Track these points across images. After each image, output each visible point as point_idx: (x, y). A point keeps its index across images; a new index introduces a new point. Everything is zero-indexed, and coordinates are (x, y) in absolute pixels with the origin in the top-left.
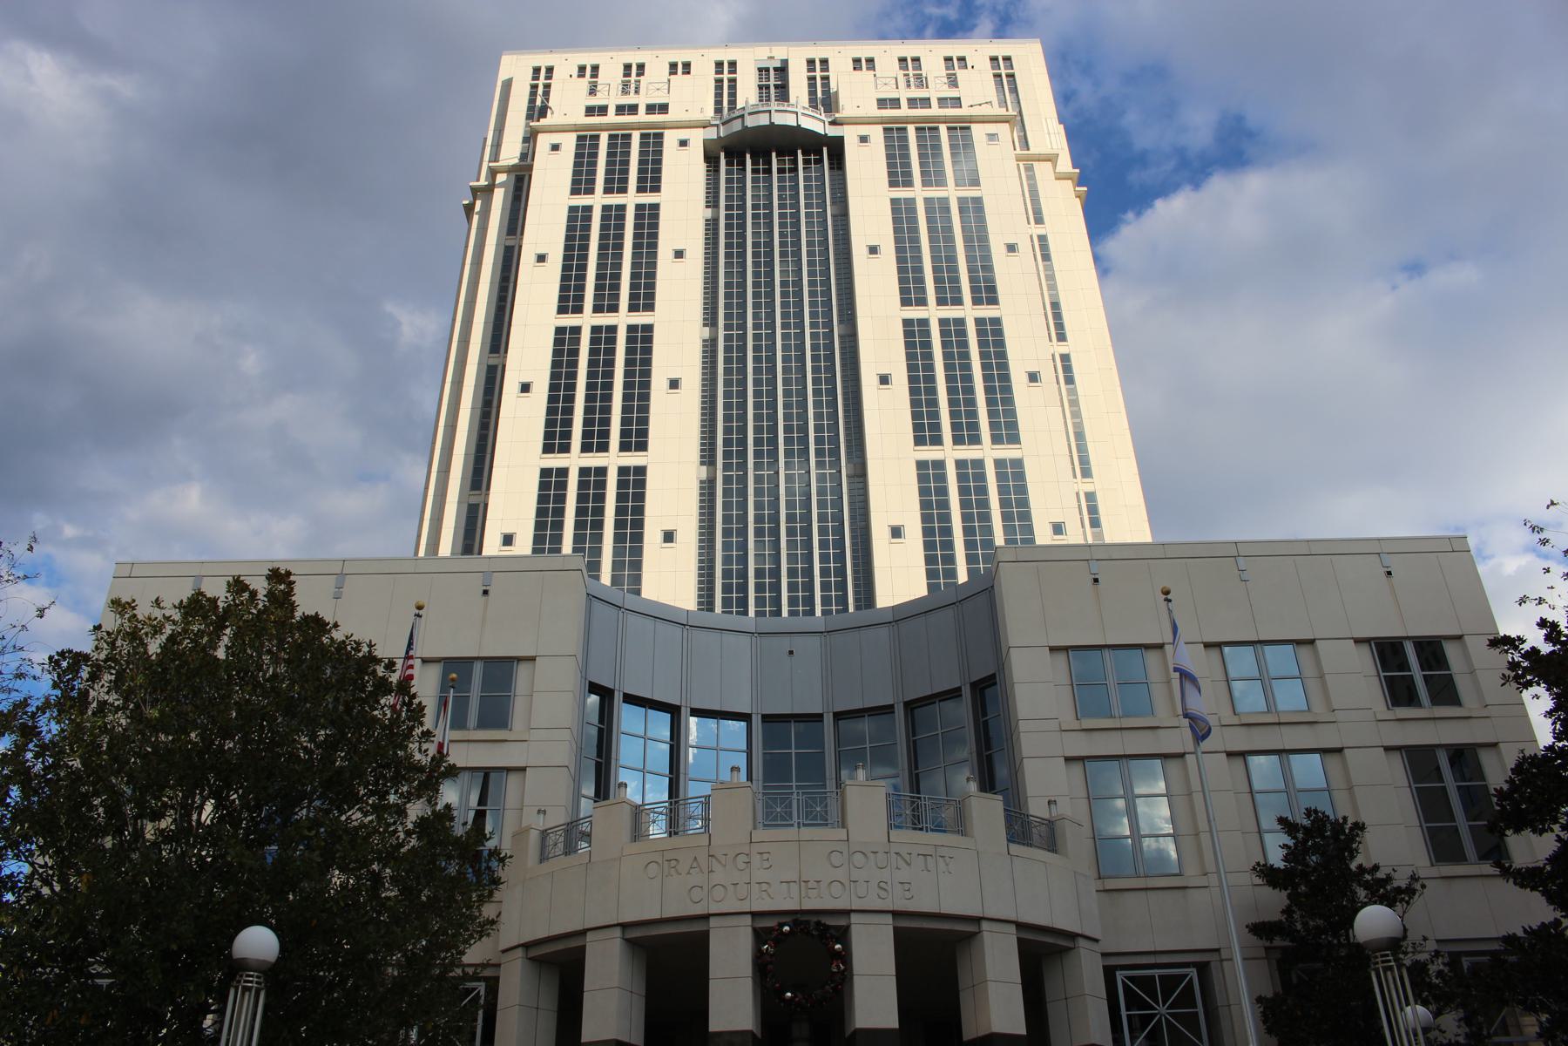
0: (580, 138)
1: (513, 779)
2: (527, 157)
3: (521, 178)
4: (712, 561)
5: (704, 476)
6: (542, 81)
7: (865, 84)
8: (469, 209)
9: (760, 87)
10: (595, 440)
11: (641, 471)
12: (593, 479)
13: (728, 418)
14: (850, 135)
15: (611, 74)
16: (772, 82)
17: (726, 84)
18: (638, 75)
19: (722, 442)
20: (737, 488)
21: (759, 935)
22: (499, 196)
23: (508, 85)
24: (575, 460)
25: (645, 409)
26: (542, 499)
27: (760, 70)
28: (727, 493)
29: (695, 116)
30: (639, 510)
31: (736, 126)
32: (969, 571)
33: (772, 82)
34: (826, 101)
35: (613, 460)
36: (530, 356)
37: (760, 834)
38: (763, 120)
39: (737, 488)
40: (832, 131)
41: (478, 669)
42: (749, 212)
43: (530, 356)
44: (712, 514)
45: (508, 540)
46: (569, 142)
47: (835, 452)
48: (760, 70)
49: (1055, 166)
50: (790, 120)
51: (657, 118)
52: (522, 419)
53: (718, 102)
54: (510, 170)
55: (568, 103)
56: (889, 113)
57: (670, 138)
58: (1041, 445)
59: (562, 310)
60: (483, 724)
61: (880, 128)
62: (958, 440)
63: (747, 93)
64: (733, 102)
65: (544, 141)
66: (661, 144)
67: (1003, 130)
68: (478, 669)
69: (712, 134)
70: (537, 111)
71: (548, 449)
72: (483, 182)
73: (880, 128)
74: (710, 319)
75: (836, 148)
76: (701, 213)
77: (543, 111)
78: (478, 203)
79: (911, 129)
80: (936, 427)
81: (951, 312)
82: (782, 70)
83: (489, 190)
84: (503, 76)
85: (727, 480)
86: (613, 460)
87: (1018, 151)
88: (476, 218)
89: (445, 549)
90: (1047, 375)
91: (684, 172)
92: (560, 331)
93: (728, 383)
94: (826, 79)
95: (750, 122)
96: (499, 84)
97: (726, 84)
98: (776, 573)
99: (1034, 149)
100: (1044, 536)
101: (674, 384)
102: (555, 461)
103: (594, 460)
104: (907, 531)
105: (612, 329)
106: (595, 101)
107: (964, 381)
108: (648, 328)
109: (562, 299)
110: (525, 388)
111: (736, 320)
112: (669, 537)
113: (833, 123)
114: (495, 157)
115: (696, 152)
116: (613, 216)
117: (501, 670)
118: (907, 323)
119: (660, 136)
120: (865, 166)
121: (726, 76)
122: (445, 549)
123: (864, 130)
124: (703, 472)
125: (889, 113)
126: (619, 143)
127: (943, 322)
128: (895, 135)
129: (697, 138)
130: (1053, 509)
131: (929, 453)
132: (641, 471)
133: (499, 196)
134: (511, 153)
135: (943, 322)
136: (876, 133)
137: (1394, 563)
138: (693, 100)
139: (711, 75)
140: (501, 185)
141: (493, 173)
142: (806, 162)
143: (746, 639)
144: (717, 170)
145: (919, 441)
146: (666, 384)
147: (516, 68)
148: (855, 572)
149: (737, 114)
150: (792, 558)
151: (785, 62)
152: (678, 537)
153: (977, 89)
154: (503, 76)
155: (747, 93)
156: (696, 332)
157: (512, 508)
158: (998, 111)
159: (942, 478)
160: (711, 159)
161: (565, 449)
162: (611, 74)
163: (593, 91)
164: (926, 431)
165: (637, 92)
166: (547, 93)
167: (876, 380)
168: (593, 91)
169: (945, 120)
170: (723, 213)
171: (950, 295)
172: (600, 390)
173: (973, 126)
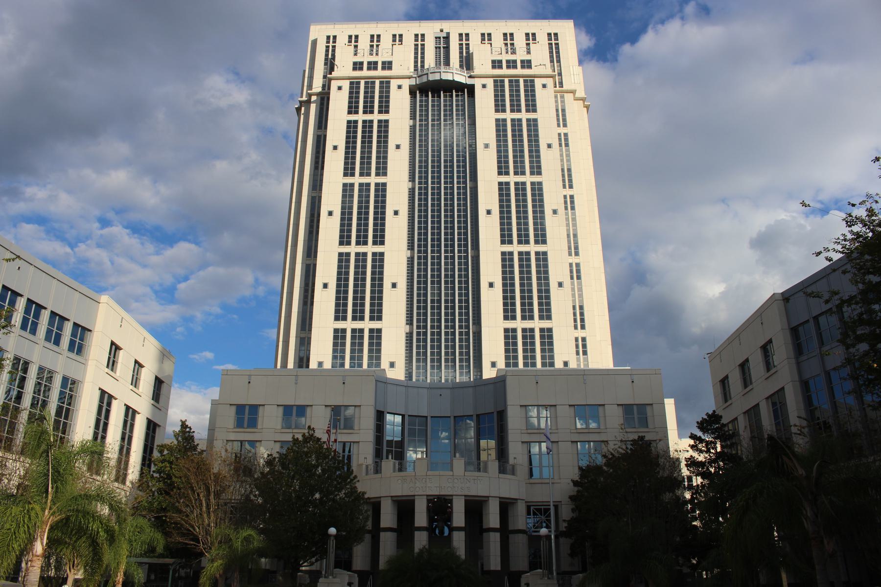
0: (351, 83)
2: (327, 86)
3: (324, 99)
4: (413, 240)
5: (409, 255)
6: (331, 44)
7: (486, 43)
8: (298, 110)
9: (436, 48)
10: (368, 110)
11: (382, 254)
12: (368, 125)
13: (420, 141)
14: (478, 83)
15: (364, 43)
16: (442, 46)
17: (420, 47)
19: (417, 240)
20: (424, 129)
21: (429, 501)
22: (313, 108)
23: (315, 42)
26: (342, 231)
27: (436, 38)
28: (420, 131)
30: (384, 202)
31: (424, 79)
33: (442, 46)
34: (467, 62)
36: (326, 270)
37: (429, 473)
38: (437, 77)
39: (423, 260)
40: (470, 82)
42: (430, 186)
43: (326, 270)
44: (412, 285)
45: (340, 88)
46: (346, 85)
47: (466, 246)
48: (436, 38)
49: (574, 94)
50: (449, 77)
51: (387, 73)
52: (324, 302)
53: (416, 66)
54: (317, 94)
56: (497, 72)
57: (394, 84)
58: (561, 323)
59: (350, 113)
61: (491, 80)
63: (430, 60)
64: (423, 66)
65: (334, 85)
66: (389, 87)
67: (549, 82)
69: (413, 82)
70: (330, 65)
71: (341, 243)
72: (304, 98)
73: (491, 80)
74: (412, 179)
75: (471, 89)
76: (404, 329)
77: (332, 69)
78: (303, 109)
79: (506, 80)
80: (504, 106)
81: (516, 116)
82: (447, 38)
83: (308, 102)
84: (312, 38)
85: (421, 125)
86: (376, 117)
87: (558, 88)
88: (302, 116)
89: (291, 365)
90: (556, 145)
91: (400, 101)
93: (420, 146)
94: (468, 45)
95: (432, 77)
96: (310, 42)
97: (420, 47)
98: (439, 301)
99: (565, 87)
100: (558, 365)
101: (396, 213)
104: (493, 212)
105: (371, 122)
106: (358, 59)
107: (528, 288)
108: (387, 121)
109: (350, 107)
110: (335, 148)
111: (423, 246)
112: (394, 285)
113: (470, 77)
114: (310, 86)
115: (406, 90)
116: (368, 125)
118: (497, 120)
119: (389, 83)
120: (484, 99)
121: (420, 43)
122: (291, 365)
124: (410, 185)
125: (497, 72)
126: (370, 86)
127: (513, 120)
128: (499, 85)
129: (406, 84)
130: (564, 353)
131: (504, 179)
132: (382, 254)
133: (313, 108)
134: (317, 87)
135: (513, 120)
136: (490, 83)
138: (403, 62)
139: (412, 42)
140: (314, 102)
141: (310, 96)
142: (457, 96)
143: (426, 390)
144: (415, 97)
145: (500, 173)
146: (393, 213)
147: (318, 32)
148: (473, 288)
149: (425, 72)
150: (446, 295)
151: (448, 34)
152: (402, 147)
153: (540, 54)
154: (312, 38)
155: (430, 60)
156: (406, 185)
157: (321, 351)
158: (549, 71)
159: (508, 189)
160: (412, 93)
161: (357, 112)
162: (364, 43)
164: (506, 238)
165: (377, 54)
166: (334, 51)
167: (485, 212)
168: (356, 54)
169: (522, 76)
170: (418, 123)
171: (515, 108)
172: (360, 290)
173: (536, 80)
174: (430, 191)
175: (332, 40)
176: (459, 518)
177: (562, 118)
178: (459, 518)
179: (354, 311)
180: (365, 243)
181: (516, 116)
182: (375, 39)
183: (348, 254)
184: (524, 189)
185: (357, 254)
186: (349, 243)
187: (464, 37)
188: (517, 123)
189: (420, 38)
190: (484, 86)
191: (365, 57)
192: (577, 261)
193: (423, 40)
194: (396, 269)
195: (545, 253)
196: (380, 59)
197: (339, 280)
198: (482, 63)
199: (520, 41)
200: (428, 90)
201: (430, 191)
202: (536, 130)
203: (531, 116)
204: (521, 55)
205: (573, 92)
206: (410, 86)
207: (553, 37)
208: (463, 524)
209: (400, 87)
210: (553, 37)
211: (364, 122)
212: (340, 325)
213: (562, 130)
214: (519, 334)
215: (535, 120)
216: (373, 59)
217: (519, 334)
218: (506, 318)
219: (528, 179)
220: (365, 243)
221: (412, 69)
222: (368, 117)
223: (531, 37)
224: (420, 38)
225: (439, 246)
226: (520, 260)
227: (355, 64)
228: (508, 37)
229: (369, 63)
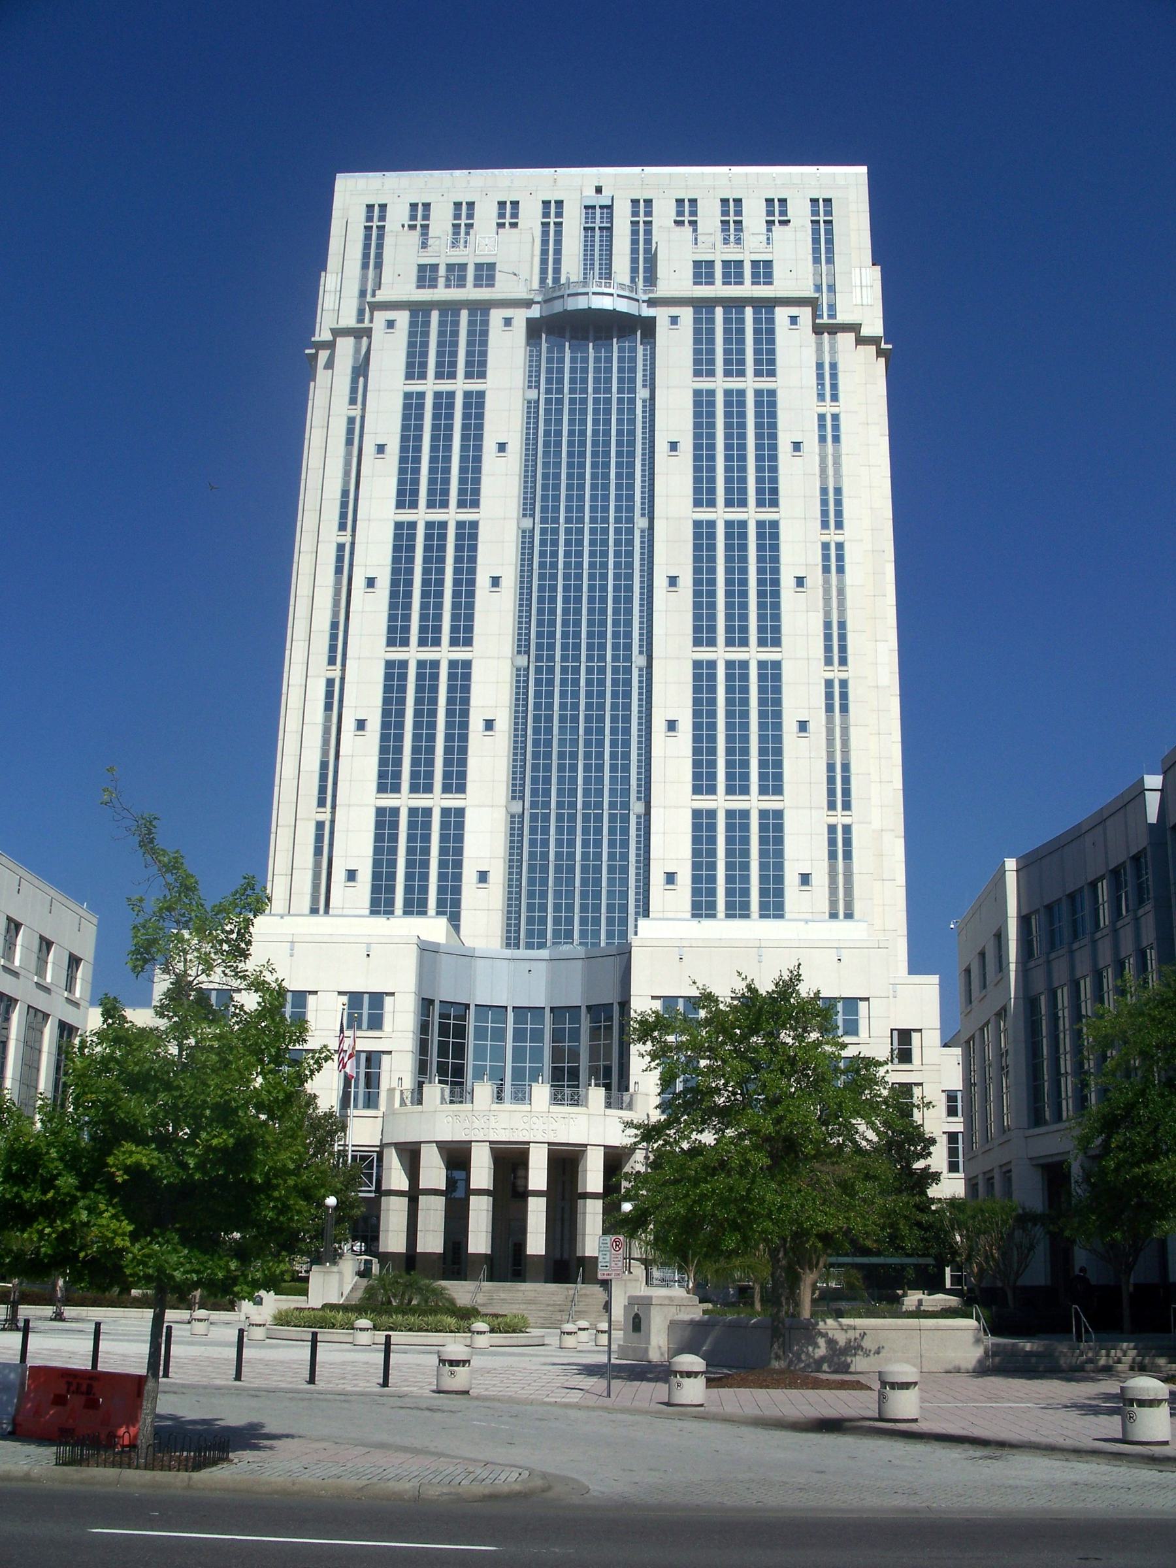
1: (385, 1058)
10: (428, 670)
14: (662, 315)
15: (441, 221)
18: (467, 233)
24: (430, 386)
25: (484, 343)
29: (521, 293)
31: (557, 307)
32: (743, 313)
33: (597, 225)
34: (647, 266)
35: (460, 385)
38: (581, 303)
39: (554, 406)
40: (647, 312)
41: (366, 997)
45: (391, 324)
50: (606, 303)
55: (402, 256)
60: (370, 1028)
62: (728, 373)
64: (557, 271)
67: (805, 313)
68: (366, 997)
69: (535, 312)
75: (648, 327)
86: (452, 515)
91: (508, 348)
92: (408, 396)
102: (416, 387)
103: (445, 386)
108: (474, 525)
117: (377, 999)
120: (674, 345)
123: (674, 311)
129: (520, 317)
137: (845, 954)
138: (519, 274)
162: (441, 221)
163: (424, 245)
168: (424, 245)
174: (562, 537)
175: (376, 212)
176: (538, 1177)
177: (828, 381)
178: (538, 1177)
179: (431, 492)
180: (445, 504)
181: (737, 654)
182: (464, 211)
183: (422, 395)
184: (742, 404)
185: (413, 812)
186: (423, 376)
187: (642, 207)
188: (737, 670)
189: (553, 208)
190: (674, 320)
191: (442, 253)
192: (843, 676)
193: (559, 214)
194: (492, 693)
195: (779, 814)
196: (468, 256)
197: (404, 438)
198: (675, 278)
199: (754, 217)
200: (566, 329)
201: (562, 537)
202: (773, 415)
203: (765, 384)
204: (752, 248)
205: (854, 328)
206: (528, 320)
207: (822, 207)
208: (543, 1187)
209: (508, 322)
210: (822, 207)
211: (429, 525)
212: (389, 801)
213: (828, 409)
214: (720, 399)
215: (772, 393)
216: (457, 256)
217: (720, 399)
218: (697, 790)
219: (754, 802)
220: (452, 375)
221: (536, 285)
222: (437, 516)
223: (777, 209)
224: (553, 208)
225: (577, 646)
226: (728, 536)
227: (422, 268)
228: (732, 207)
229: (450, 267)
